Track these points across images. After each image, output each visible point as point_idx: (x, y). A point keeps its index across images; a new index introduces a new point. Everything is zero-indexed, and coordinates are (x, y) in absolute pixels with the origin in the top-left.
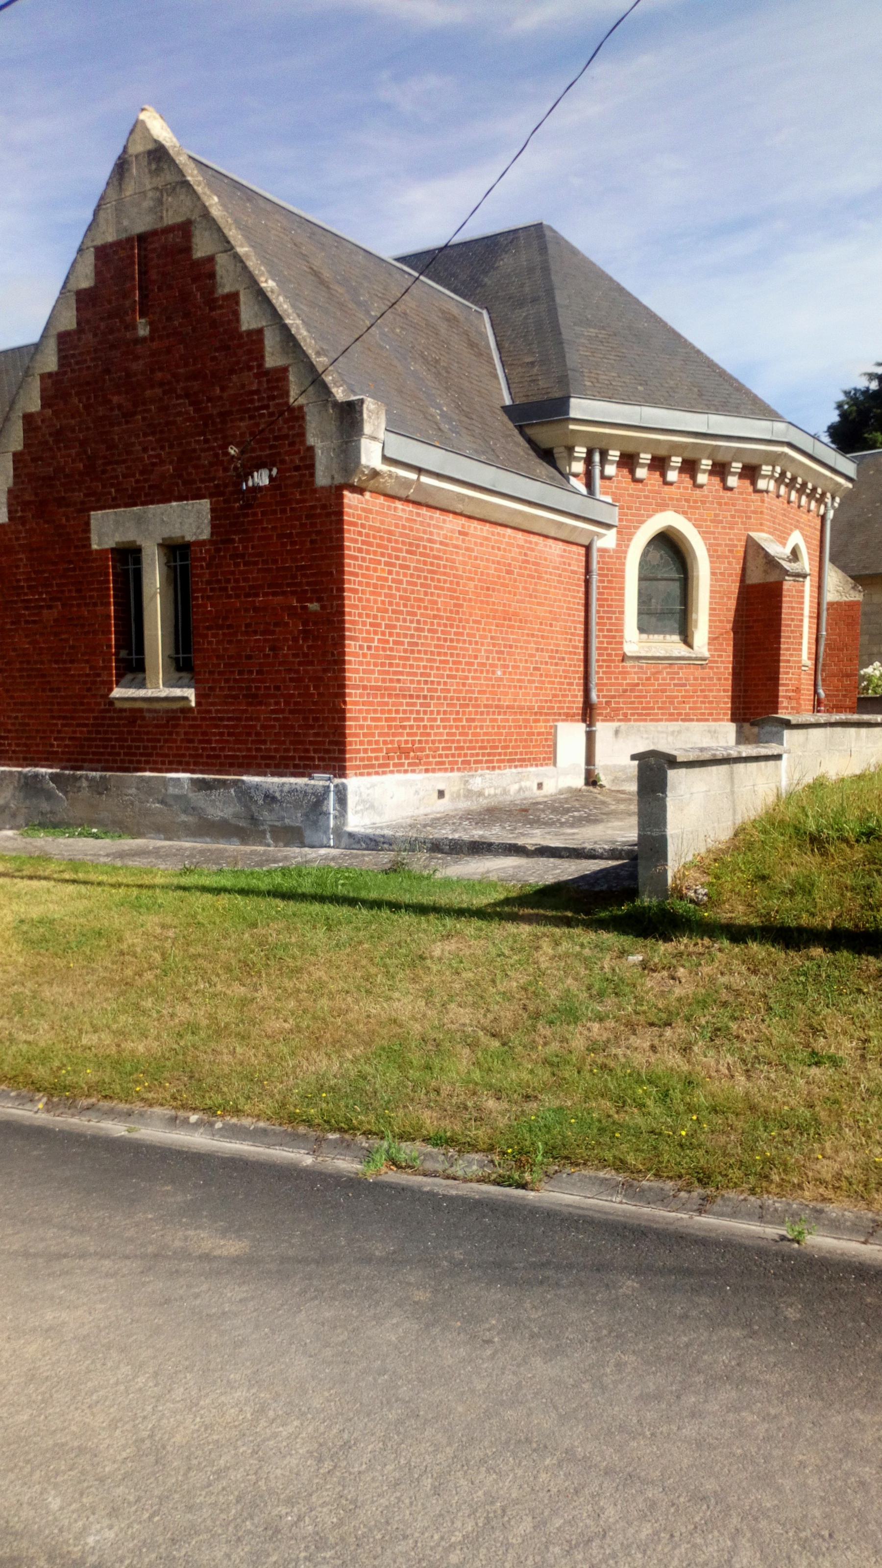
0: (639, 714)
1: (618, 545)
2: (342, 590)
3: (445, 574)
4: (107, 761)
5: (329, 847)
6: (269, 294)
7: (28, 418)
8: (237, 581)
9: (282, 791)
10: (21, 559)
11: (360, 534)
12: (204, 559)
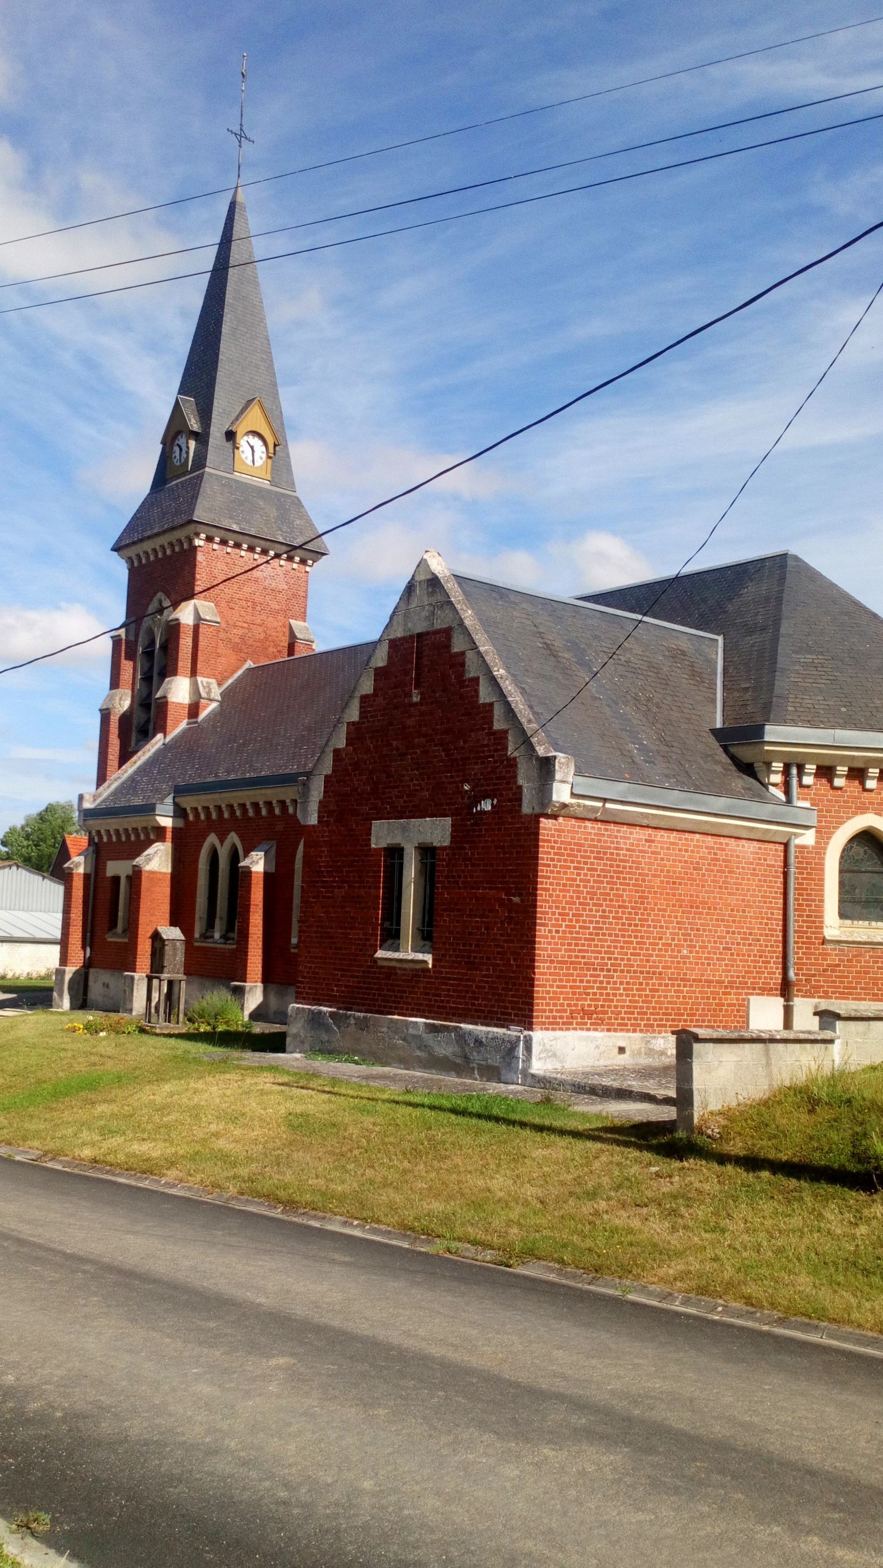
0: (840, 993)
1: (817, 842)
2: (536, 889)
3: (630, 873)
4: (369, 1005)
5: (518, 1084)
6: (499, 680)
7: (336, 752)
8: (465, 877)
9: (487, 1038)
10: (323, 852)
11: (553, 848)
12: (444, 860)
